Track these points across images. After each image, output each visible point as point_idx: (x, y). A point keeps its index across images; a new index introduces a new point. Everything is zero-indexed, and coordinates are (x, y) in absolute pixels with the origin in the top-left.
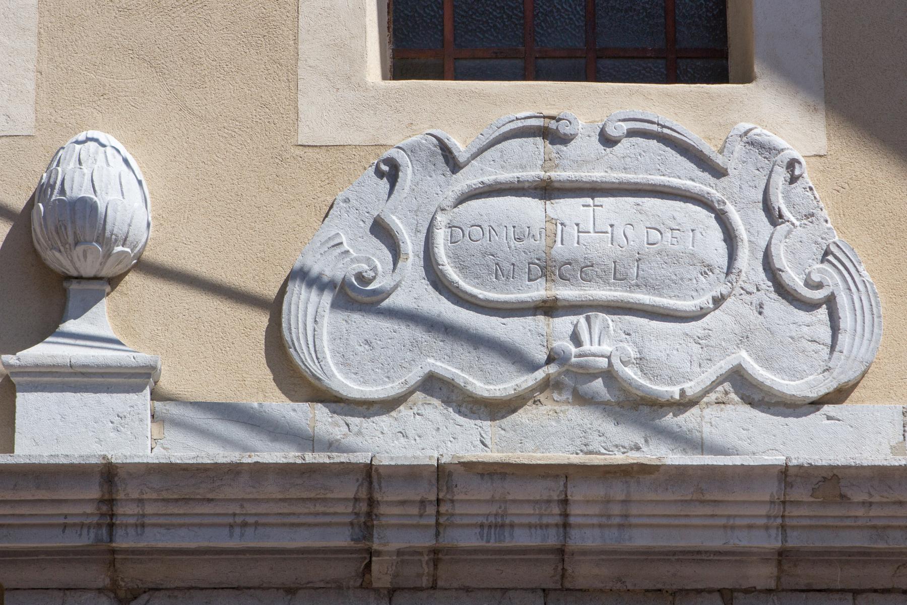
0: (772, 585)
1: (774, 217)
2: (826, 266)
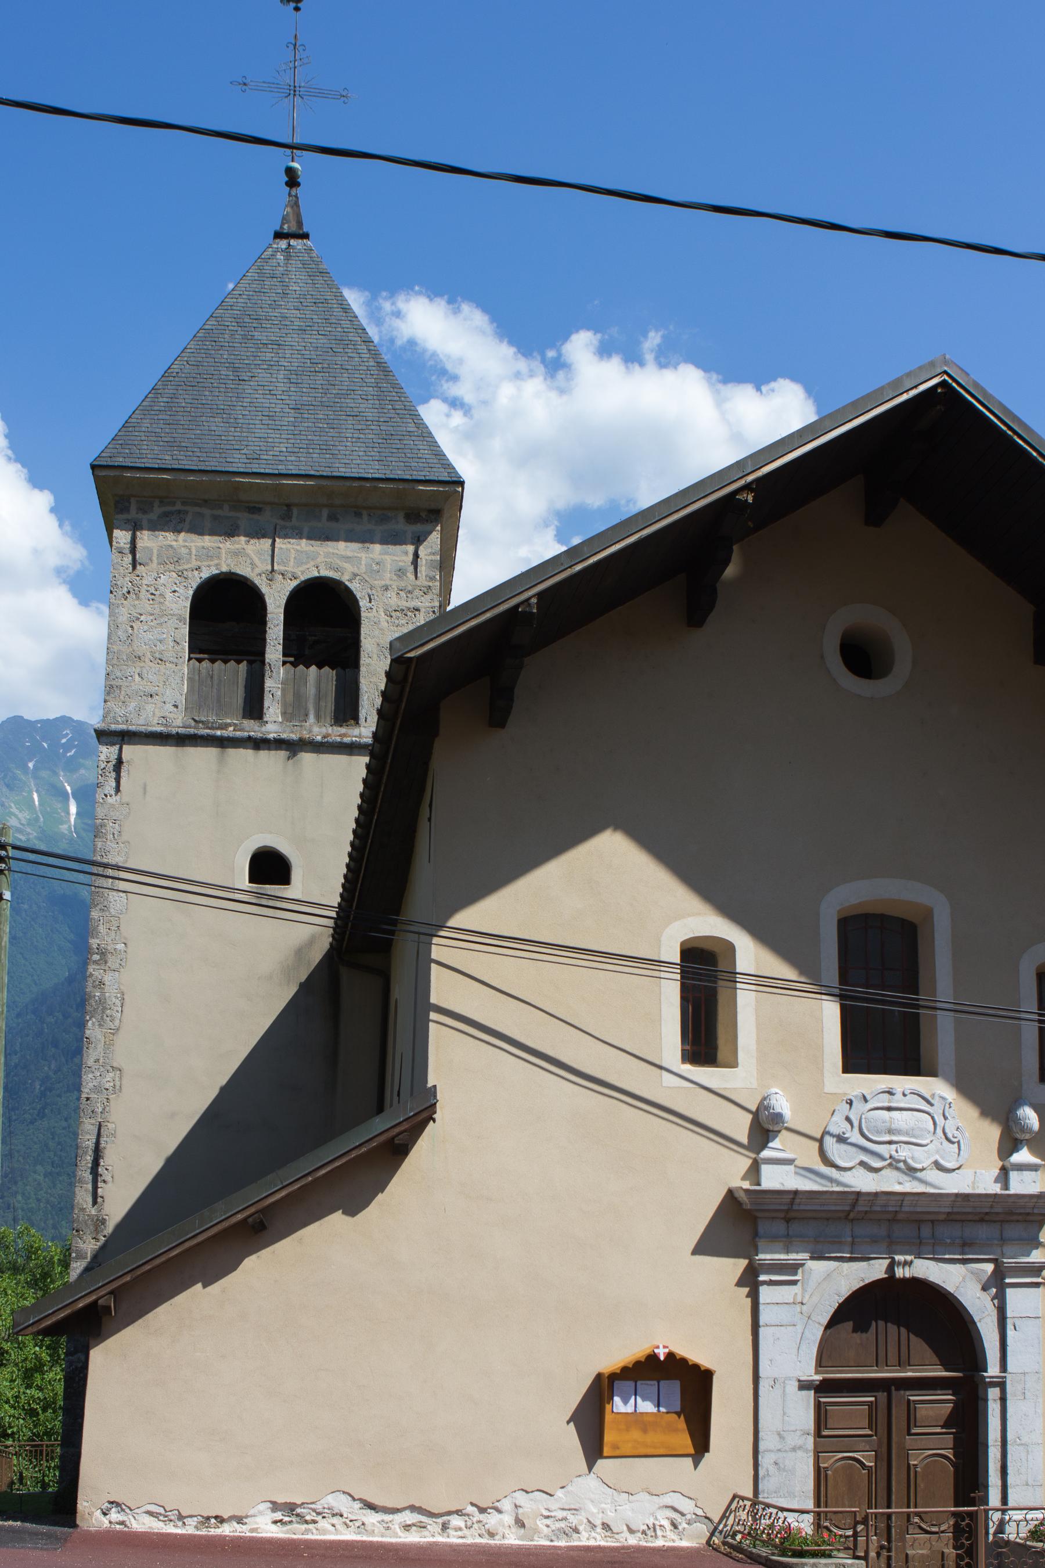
1: (945, 1118)
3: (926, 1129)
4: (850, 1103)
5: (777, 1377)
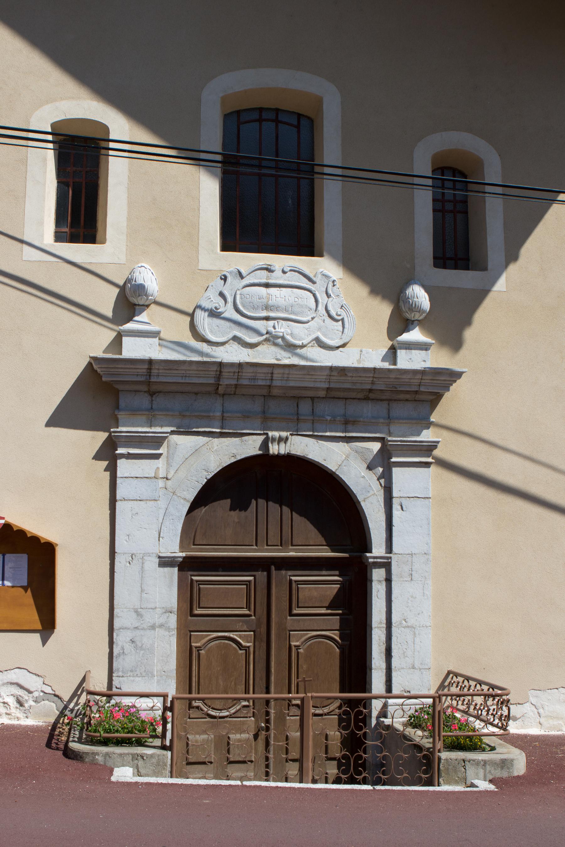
0: (324, 396)
1: (328, 296)
2: (342, 310)
3: (306, 305)
4: (225, 279)
5: (135, 552)
